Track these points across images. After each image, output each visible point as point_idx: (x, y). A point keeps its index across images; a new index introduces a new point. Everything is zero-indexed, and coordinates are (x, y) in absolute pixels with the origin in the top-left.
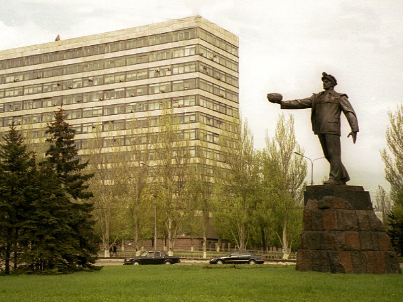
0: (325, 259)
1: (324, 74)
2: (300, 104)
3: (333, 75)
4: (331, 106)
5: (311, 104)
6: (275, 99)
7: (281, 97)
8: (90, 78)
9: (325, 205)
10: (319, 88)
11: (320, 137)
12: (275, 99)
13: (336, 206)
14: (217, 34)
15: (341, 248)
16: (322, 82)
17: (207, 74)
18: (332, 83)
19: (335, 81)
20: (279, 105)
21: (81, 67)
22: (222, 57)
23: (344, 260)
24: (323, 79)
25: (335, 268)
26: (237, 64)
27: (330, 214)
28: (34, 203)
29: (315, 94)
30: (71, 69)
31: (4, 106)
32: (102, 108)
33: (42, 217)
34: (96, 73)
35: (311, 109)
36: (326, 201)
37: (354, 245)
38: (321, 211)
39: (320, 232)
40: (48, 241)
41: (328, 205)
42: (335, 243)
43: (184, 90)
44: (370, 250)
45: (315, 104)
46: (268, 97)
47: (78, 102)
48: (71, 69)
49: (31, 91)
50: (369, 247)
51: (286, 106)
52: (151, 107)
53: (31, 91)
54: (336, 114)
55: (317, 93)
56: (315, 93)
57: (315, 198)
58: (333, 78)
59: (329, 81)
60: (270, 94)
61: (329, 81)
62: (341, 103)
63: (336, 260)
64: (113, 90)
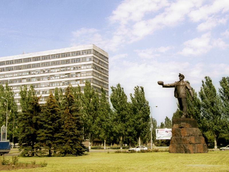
0: (182, 147)
1: (180, 74)
2: (170, 86)
3: (183, 74)
4: (183, 87)
5: (174, 86)
6: (161, 84)
7: (163, 83)
8: (44, 70)
9: (182, 126)
10: (178, 79)
11: (178, 99)
12: (161, 84)
13: (186, 127)
14: (100, 52)
15: (189, 143)
16: (179, 78)
17: (96, 69)
18: (183, 78)
19: (184, 77)
20: (162, 86)
21: (38, 65)
22: (102, 62)
23: (190, 147)
24: (179, 76)
25: (186, 151)
26: (107, 65)
27: (184, 130)
28: (62, 127)
29: (176, 82)
30: (34, 66)
31: (50, 84)
32: (49, 83)
33: (66, 132)
34: (46, 68)
35: (174, 88)
36: (182, 124)
37: (193, 142)
38: (180, 129)
39: (180, 137)
40: (70, 143)
41: (183, 126)
42: (187, 141)
43: (86, 76)
44: (198, 143)
45: (177, 86)
46: (158, 83)
47: (39, 80)
48: (34, 66)
49: (16, 75)
50: (198, 142)
51: (164, 87)
52: (23, 81)
53: (16, 75)
54: (185, 90)
55: (177, 81)
56: (176, 81)
57: (177, 123)
58: (183, 75)
59: (181, 77)
60: (159, 82)
61: (181, 77)
62: (187, 86)
63: (187, 148)
64: (54, 75)
